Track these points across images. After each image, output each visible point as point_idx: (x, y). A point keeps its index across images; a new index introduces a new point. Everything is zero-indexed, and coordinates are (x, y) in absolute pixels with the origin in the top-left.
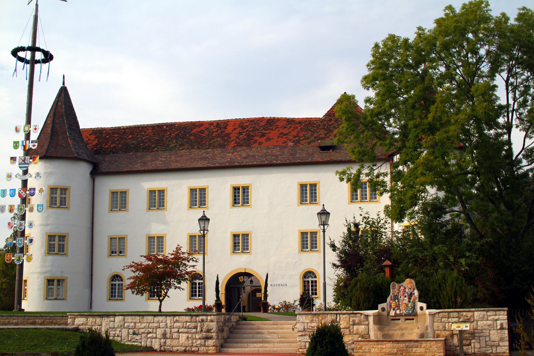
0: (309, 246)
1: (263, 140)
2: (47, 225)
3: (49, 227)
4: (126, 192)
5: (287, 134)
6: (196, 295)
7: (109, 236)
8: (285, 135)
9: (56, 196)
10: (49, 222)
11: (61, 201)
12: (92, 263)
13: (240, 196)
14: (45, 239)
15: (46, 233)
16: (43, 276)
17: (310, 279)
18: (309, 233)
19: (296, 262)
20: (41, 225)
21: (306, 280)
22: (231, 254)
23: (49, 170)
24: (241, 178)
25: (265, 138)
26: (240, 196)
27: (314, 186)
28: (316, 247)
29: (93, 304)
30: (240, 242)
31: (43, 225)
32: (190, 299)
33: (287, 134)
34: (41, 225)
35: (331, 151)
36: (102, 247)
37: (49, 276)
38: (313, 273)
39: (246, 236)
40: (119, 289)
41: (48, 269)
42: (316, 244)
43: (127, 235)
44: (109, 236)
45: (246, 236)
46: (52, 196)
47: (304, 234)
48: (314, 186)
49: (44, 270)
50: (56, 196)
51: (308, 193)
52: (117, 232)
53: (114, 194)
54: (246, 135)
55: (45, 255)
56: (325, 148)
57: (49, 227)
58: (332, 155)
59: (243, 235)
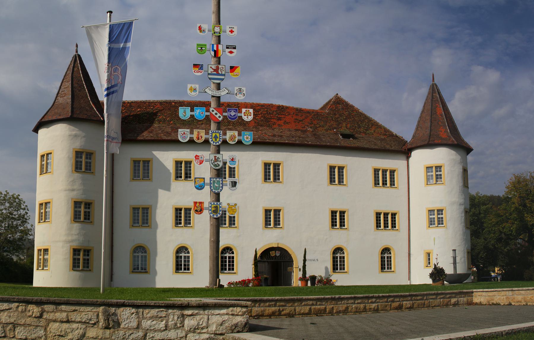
0: (183, 221)
1: (281, 122)
2: (73, 190)
3: (75, 193)
4: (149, 161)
5: (302, 121)
6: (226, 270)
7: (130, 206)
8: (300, 121)
9: (81, 160)
10: (75, 187)
11: (86, 166)
12: (112, 233)
13: (272, 172)
14: (71, 205)
15: (72, 199)
16: (68, 245)
17: (183, 255)
18: (141, 209)
19: (327, 239)
20: (65, 190)
21: (136, 254)
22: (263, 229)
23: (74, 133)
24: (272, 156)
25: (282, 121)
26: (272, 172)
27: (277, 166)
28: (190, 224)
29: (115, 277)
30: (272, 218)
31: (69, 190)
32: (382, 272)
33: (302, 121)
34: (65, 190)
35: (351, 139)
36: (124, 216)
37: (75, 245)
38: (186, 249)
39: (277, 212)
40: (340, 261)
41: (75, 237)
42: (190, 220)
43: (151, 206)
44: (130, 206)
45: (277, 212)
46: (77, 159)
47: (178, 210)
48: (277, 166)
49: (70, 238)
50: (81, 160)
51: (336, 175)
52: (140, 202)
53: (136, 163)
54: (262, 117)
55: (71, 223)
56: (346, 136)
57: (75, 193)
58: (351, 142)
59: (341, 212)
